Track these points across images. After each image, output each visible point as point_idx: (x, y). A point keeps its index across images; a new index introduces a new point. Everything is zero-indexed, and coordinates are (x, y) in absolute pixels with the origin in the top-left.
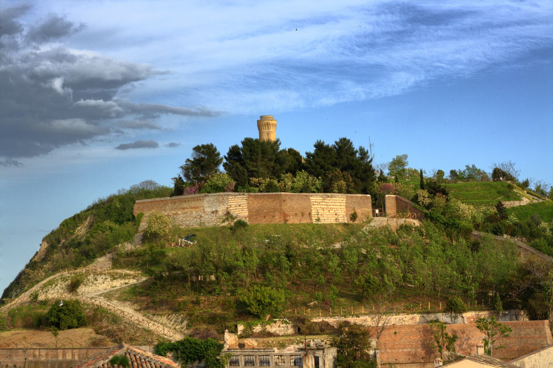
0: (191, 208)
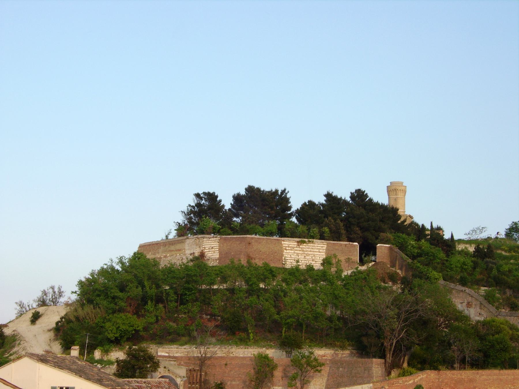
0: (176, 250)
